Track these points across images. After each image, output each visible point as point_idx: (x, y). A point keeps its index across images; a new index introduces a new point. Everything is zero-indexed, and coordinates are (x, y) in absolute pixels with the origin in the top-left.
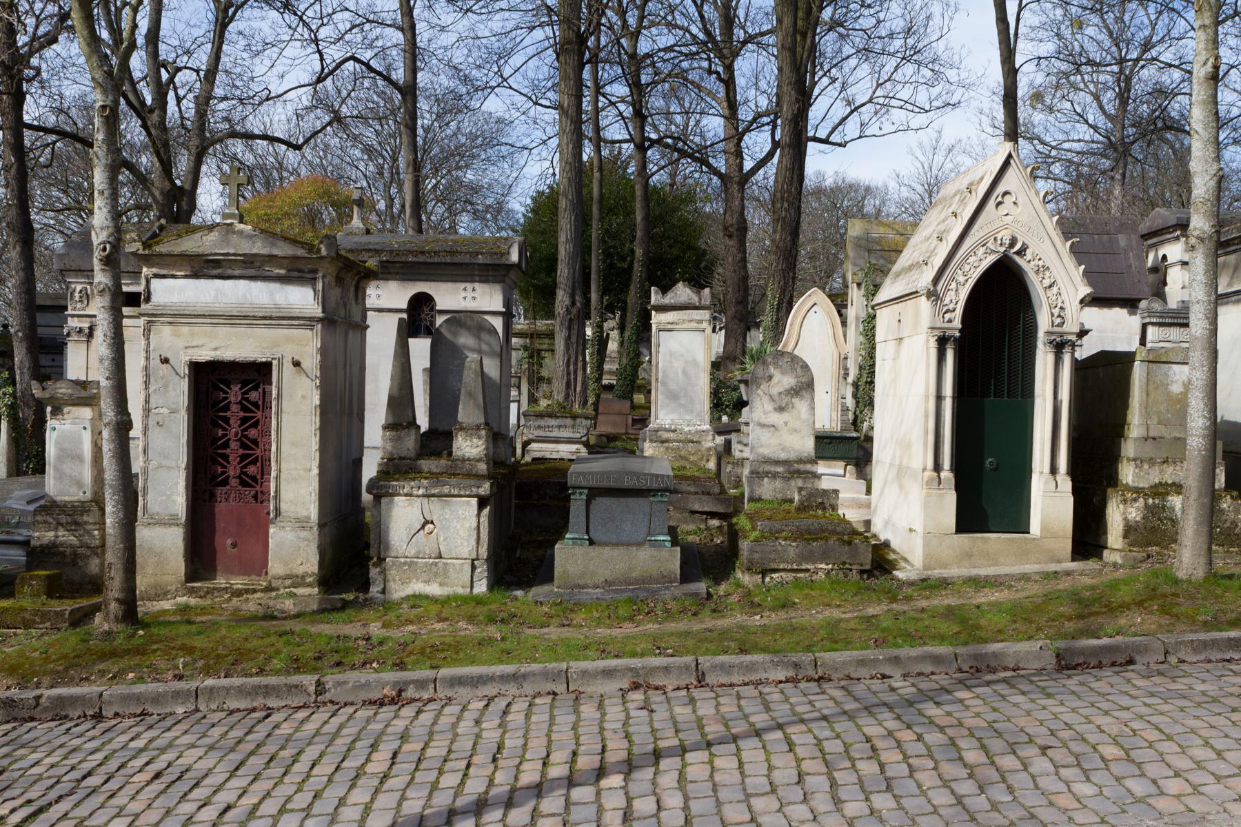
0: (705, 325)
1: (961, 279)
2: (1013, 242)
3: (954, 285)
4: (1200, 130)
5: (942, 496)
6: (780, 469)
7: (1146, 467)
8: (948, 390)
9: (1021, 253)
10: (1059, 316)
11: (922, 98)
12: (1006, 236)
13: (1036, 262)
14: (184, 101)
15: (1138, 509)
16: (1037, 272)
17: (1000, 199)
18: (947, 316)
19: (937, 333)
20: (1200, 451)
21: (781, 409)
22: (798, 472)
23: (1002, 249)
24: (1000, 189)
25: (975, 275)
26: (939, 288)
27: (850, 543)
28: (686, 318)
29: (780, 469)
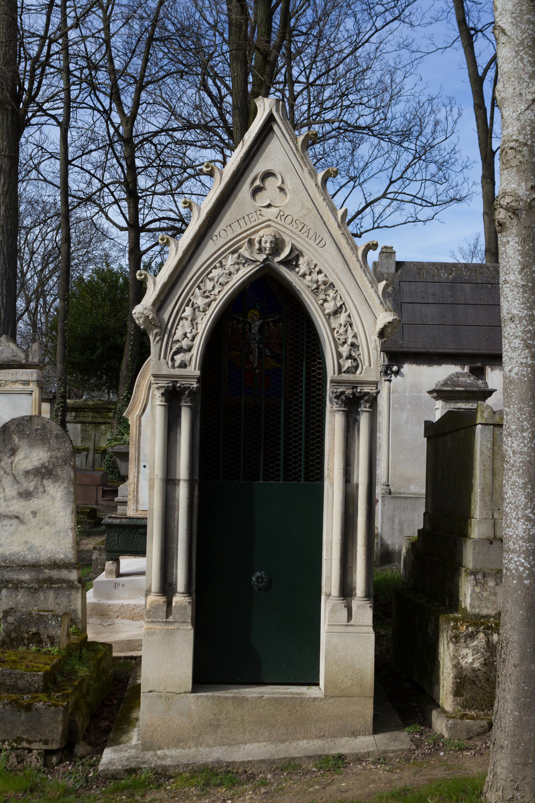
0: (33, 387)
1: (200, 302)
2: (277, 245)
3: (188, 311)
4: (508, 28)
5: (170, 633)
6: (25, 577)
7: (491, 583)
8: (183, 470)
9: (292, 262)
10: (350, 357)
11: (429, 192)
12: (266, 237)
13: (314, 276)
14: (36, 255)
15: (476, 650)
16: (316, 291)
17: (258, 183)
18: (179, 358)
19: (163, 383)
20: (520, 578)
21: (26, 495)
22: (50, 581)
23: (261, 257)
24: (260, 167)
25: (222, 296)
26: (166, 316)
27: (28, 708)
28: (10, 378)
29: (25, 577)
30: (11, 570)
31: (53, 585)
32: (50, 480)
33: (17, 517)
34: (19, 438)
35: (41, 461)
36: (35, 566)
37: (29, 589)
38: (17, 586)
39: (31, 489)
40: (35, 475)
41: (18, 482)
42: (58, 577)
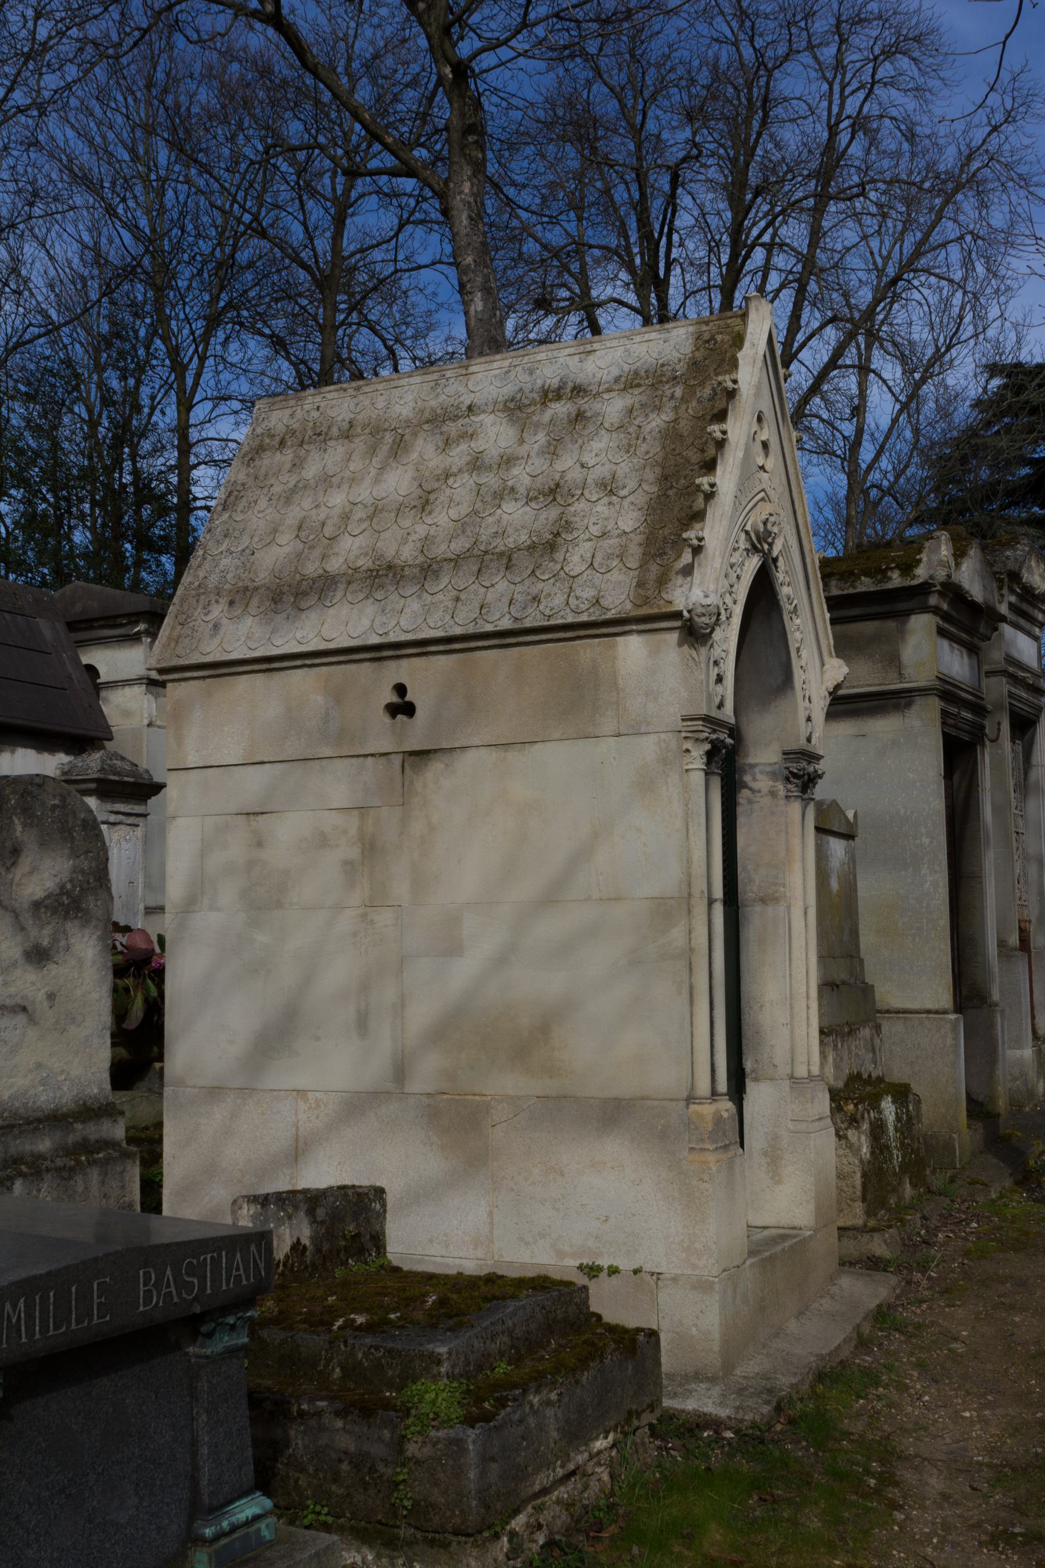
6: (44, 1145)
21: (38, 956)
22: (86, 1147)
29: (44, 1145)
30: (21, 1132)
31: (96, 1156)
32: (77, 922)
33: (24, 1009)
34: (24, 825)
35: (57, 880)
36: (56, 1119)
37: (59, 1170)
38: (34, 1168)
39: (45, 943)
40: (55, 912)
41: (23, 929)
42: (97, 1136)
